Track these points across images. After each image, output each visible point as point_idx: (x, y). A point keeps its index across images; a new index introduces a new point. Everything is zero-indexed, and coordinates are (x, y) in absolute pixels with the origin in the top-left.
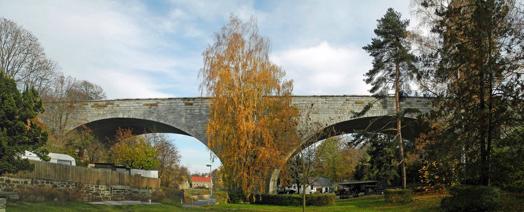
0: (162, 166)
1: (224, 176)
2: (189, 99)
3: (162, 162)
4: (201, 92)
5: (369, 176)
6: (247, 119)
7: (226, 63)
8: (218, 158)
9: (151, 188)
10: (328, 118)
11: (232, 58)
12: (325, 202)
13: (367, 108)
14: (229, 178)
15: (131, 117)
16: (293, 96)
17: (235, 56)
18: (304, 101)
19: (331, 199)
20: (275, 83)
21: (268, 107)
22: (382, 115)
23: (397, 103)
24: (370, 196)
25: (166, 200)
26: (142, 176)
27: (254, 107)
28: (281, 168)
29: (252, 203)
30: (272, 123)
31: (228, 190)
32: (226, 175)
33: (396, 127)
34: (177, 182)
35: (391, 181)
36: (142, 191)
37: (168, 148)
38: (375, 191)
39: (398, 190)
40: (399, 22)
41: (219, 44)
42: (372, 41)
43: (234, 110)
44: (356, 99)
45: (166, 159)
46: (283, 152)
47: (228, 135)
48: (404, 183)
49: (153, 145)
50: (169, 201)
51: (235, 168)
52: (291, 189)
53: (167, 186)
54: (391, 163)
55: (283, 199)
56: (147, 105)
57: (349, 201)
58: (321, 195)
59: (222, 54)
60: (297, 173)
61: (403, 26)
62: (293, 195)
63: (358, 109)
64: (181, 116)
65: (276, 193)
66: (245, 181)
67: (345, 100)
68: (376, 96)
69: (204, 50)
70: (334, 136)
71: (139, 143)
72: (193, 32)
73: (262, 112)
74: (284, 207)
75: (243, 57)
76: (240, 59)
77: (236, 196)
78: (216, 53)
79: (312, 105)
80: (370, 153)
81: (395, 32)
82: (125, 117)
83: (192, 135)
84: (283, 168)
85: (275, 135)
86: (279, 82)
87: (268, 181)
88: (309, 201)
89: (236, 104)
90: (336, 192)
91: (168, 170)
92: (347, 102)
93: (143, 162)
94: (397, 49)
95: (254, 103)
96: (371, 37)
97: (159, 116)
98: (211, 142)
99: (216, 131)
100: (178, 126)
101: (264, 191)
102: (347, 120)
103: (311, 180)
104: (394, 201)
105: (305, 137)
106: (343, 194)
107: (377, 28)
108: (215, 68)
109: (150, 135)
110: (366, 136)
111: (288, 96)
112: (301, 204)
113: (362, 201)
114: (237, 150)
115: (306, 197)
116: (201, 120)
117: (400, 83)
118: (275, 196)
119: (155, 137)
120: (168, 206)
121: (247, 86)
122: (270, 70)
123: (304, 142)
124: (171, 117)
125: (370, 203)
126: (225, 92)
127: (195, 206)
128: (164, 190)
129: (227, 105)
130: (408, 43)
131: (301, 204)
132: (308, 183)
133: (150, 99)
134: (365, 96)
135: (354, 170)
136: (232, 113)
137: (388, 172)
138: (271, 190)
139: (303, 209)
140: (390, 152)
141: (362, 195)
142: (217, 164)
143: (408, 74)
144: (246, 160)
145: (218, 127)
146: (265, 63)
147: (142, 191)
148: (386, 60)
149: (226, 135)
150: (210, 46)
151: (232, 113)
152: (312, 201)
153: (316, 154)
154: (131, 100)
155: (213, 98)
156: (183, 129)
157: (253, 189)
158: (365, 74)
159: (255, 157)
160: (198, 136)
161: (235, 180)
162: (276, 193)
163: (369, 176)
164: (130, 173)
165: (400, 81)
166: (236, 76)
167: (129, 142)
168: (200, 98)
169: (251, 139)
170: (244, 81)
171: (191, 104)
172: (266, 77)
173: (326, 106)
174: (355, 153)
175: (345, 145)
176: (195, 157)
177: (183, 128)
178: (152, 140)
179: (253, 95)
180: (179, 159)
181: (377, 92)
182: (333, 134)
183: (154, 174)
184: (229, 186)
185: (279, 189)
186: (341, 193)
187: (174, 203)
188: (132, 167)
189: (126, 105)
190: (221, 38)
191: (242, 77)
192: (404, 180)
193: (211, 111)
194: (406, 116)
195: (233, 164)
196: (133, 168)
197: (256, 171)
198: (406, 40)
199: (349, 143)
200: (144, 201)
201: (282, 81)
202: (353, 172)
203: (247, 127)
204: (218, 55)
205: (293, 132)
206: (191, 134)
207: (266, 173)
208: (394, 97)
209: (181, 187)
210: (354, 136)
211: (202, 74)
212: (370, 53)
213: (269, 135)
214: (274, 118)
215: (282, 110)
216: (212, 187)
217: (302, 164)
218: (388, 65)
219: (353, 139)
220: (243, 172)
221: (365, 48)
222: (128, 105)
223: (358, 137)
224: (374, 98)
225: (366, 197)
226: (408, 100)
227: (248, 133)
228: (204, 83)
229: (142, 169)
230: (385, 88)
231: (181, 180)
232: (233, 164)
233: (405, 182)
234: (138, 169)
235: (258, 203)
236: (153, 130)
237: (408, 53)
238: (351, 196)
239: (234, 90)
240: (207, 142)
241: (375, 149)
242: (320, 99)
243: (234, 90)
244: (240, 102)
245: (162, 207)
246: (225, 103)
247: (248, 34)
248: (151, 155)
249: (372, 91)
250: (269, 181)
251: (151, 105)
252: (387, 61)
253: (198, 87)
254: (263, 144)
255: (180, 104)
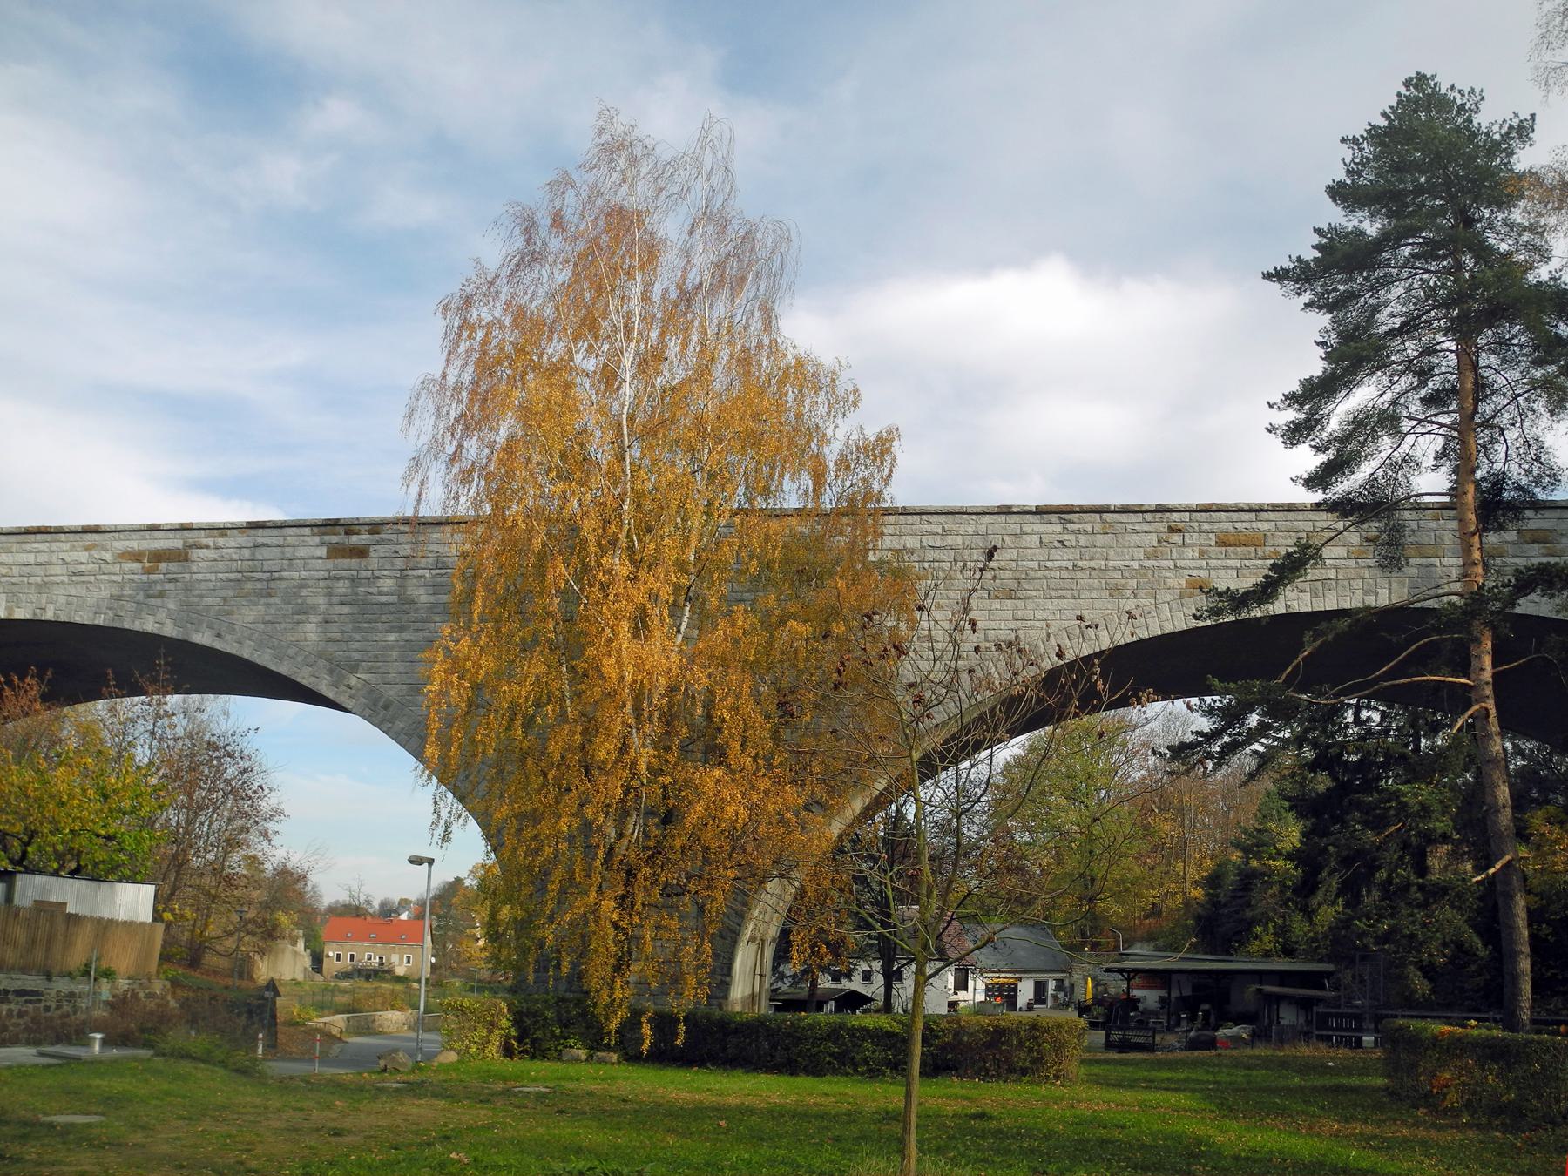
0: (179, 863)
1: (493, 914)
2: (350, 527)
3: (182, 841)
4: (414, 489)
5: (1282, 931)
6: (641, 626)
7: (555, 348)
8: (472, 822)
9: (108, 974)
10: (1068, 622)
11: (589, 325)
12: (1021, 1058)
13: (1289, 568)
14: (523, 926)
15: (49, 616)
16: (888, 512)
17: (605, 314)
18: (945, 533)
19: (1058, 1047)
20: (799, 445)
21: (754, 567)
22: (1372, 601)
23: (1465, 537)
24: (1287, 1051)
25: (181, 1036)
26: (70, 909)
27: (681, 566)
28: (799, 878)
29: (632, 1057)
30: (770, 643)
31: (513, 990)
32: (505, 912)
33: (1464, 665)
34: (248, 944)
35: (1428, 971)
36: (62, 986)
37: (219, 772)
38: (1323, 1021)
39: (1475, 1029)
40: (1474, 135)
41: (530, 258)
42: (1316, 239)
43: (579, 580)
44: (1224, 523)
45: (204, 824)
46: (821, 793)
47: (538, 704)
48: (1516, 993)
49: (142, 754)
50: (195, 1040)
51: (558, 875)
52: (846, 985)
53: (194, 962)
54: (1422, 870)
55: (799, 1040)
56: (136, 557)
57: (1161, 1064)
58: (1008, 1018)
59: (539, 305)
60: (883, 905)
61: (1493, 148)
62: (858, 1019)
63: (1238, 573)
64: (304, 610)
65: (764, 1008)
66: (606, 943)
67: (1163, 527)
68: (1342, 507)
69: (453, 288)
70: (1096, 709)
71: (73, 744)
72: (402, 205)
73: (725, 589)
74: (804, 1082)
75: (648, 319)
76: (628, 331)
77: (549, 1016)
78: (508, 303)
79: (990, 555)
80: (1303, 805)
81: (1448, 184)
82: (20, 614)
83: (348, 704)
84: (816, 876)
85: (781, 705)
86: (823, 440)
87: (728, 940)
88: (944, 1048)
89: (592, 548)
90: (1083, 1010)
91: (208, 881)
92: (1176, 538)
93: (82, 842)
94: (1459, 267)
95: (685, 544)
96: (1307, 219)
97: (190, 613)
98: (444, 742)
99: (476, 687)
100: (279, 659)
101: (703, 995)
102: (1169, 629)
103: (959, 940)
104: (1453, 1099)
105: (939, 715)
106: (1125, 1024)
107: (1341, 175)
108: (502, 373)
109: (135, 704)
110: (1280, 711)
111: (865, 511)
112: (898, 1066)
113: (1240, 1076)
114: (576, 779)
115: (927, 1027)
116: (401, 630)
117: (1484, 435)
118: (761, 1022)
119: (158, 716)
120: (185, 1066)
121: (654, 462)
122: (782, 383)
123: (934, 741)
124: (248, 615)
125: (1291, 1092)
126: (538, 491)
127: (330, 1071)
128: (175, 983)
129: (542, 556)
130: (1531, 229)
131: (898, 1066)
132: (942, 956)
133: (153, 528)
134: (1275, 508)
135: (1198, 893)
136: (565, 594)
137: (1410, 921)
138: (739, 990)
139: (908, 1096)
140: (1424, 807)
141: (1236, 1041)
142: (466, 853)
143: (1534, 385)
144: (621, 835)
145: (488, 663)
146: (760, 346)
147: (62, 986)
148: (1397, 322)
149: (527, 707)
150: (482, 271)
151: (565, 594)
152: (956, 1051)
153: (996, 804)
154: (59, 531)
155: (476, 522)
156: (305, 678)
157: (642, 983)
158: (1277, 398)
159: (668, 819)
160: (381, 713)
161: (549, 935)
162: (764, 1008)
163: (1282, 931)
164: (9, 898)
165: (1486, 424)
166: (603, 410)
167: (25, 741)
168: (406, 521)
169: (654, 728)
170: (640, 438)
171: (361, 553)
172: (755, 416)
173: (1062, 559)
174: (1204, 802)
175: (1152, 760)
176: (355, 816)
177: (306, 671)
178: (142, 727)
179: (681, 505)
180: (270, 826)
181: (1347, 485)
182: (1090, 702)
183: (133, 901)
184: (519, 969)
185: (785, 986)
186: (1114, 1017)
187: (219, 1054)
188: (24, 864)
189: (31, 558)
190: (543, 233)
191: (631, 419)
192: (1515, 978)
193: (459, 586)
194: (1534, 605)
195: (548, 851)
196: (28, 871)
197: (669, 892)
198: (1517, 215)
199: (1180, 751)
200: (68, 1040)
201: (841, 434)
202: (1187, 903)
203: (639, 667)
204: (520, 315)
205: (881, 689)
206: (343, 700)
207: (718, 903)
208: (1443, 507)
209: (263, 970)
210: (1210, 712)
211: (427, 405)
212: (1307, 297)
213: (748, 707)
214: (782, 622)
215: (823, 586)
216: (426, 973)
217: (918, 854)
218: (1412, 349)
219: (1205, 724)
220: (600, 892)
221: (1279, 276)
222: (42, 558)
223: (1231, 717)
224: (1324, 519)
225: (1262, 1051)
226: (1534, 521)
227: (638, 696)
228: (436, 447)
229: (74, 873)
230: (1395, 466)
231: (270, 934)
232: (548, 851)
233: (1526, 986)
234: (56, 873)
235: (664, 1056)
236: (154, 680)
237: (1531, 278)
238: (1171, 1039)
239: (583, 482)
240: (423, 739)
241: (1323, 782)
242: (1034, 525)
243: (583, 482)
244: (614, 542)
245: (157, 1072)
246: (537, 543)
247: (683, 209)
248: (127, 804)
249: (1315, 481)
250: (735, 943)
251: (158, 557)
252: (1408, 328)
253: (401, 470)
254: (715, 753)
255: (302, 552)
